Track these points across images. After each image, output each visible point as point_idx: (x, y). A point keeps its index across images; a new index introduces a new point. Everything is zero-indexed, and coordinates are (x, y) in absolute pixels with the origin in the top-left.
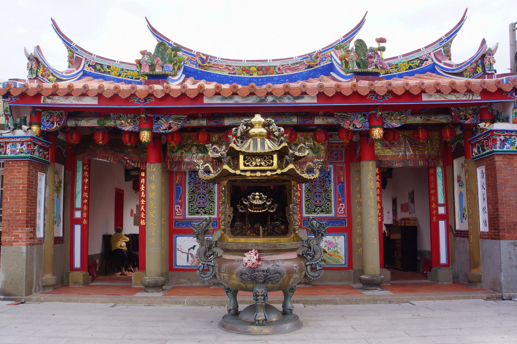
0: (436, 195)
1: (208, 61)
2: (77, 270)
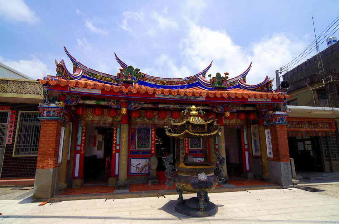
2: (77, 178)
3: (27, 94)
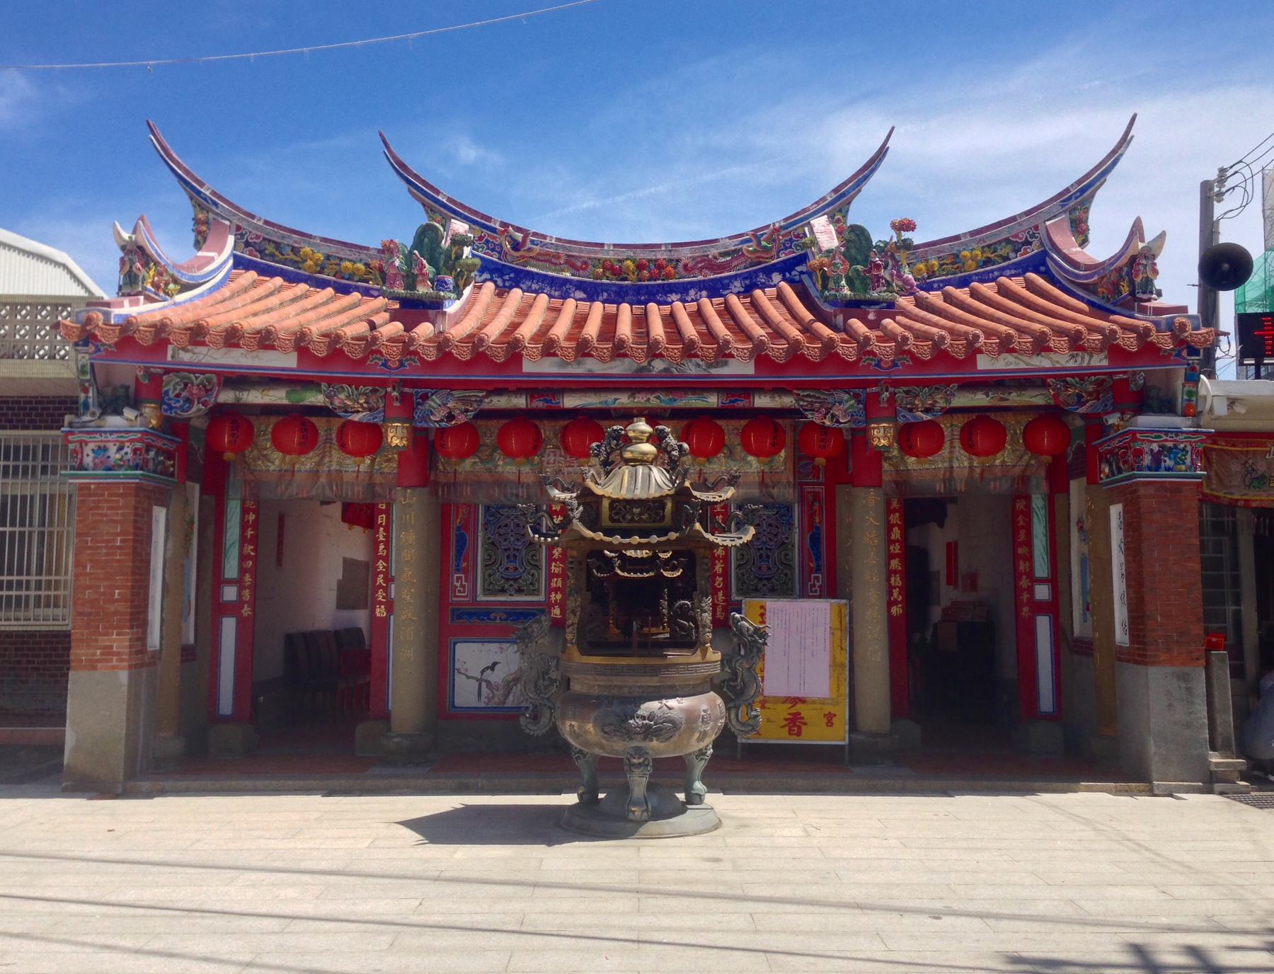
0: (1029, 558)
1: (529, 245)
2: (225, 719)
3: (10, 361)
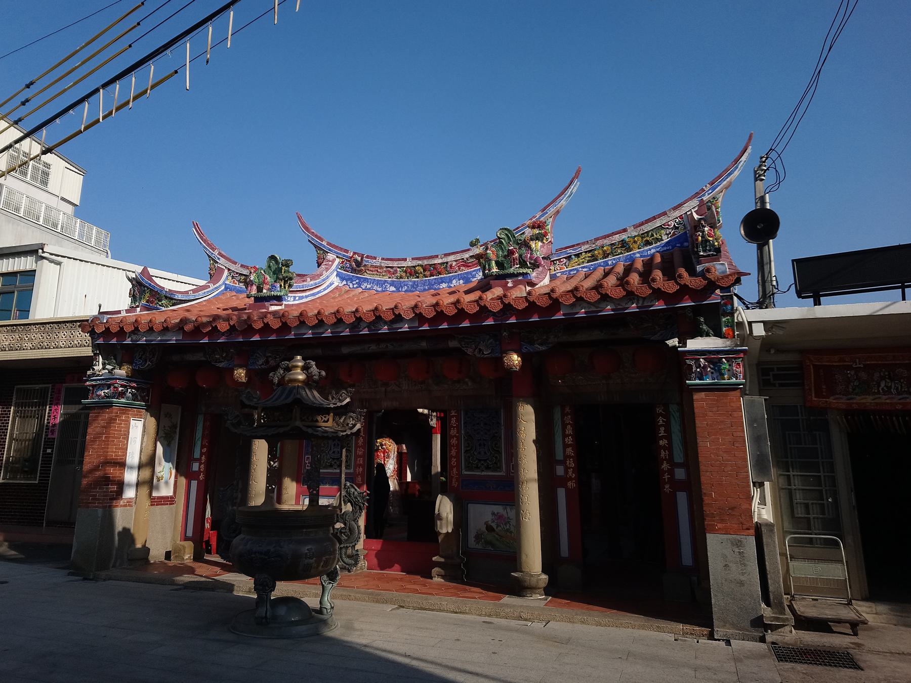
1: (364, 263)
